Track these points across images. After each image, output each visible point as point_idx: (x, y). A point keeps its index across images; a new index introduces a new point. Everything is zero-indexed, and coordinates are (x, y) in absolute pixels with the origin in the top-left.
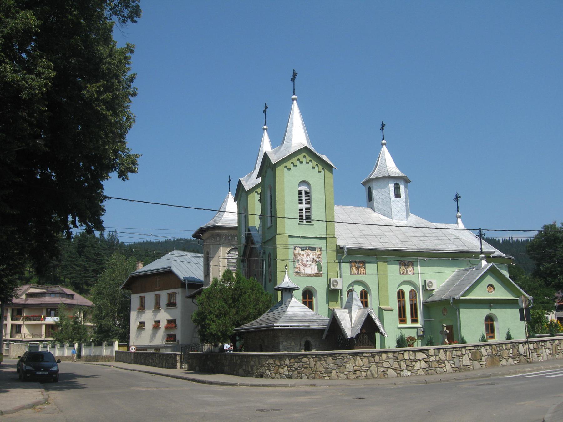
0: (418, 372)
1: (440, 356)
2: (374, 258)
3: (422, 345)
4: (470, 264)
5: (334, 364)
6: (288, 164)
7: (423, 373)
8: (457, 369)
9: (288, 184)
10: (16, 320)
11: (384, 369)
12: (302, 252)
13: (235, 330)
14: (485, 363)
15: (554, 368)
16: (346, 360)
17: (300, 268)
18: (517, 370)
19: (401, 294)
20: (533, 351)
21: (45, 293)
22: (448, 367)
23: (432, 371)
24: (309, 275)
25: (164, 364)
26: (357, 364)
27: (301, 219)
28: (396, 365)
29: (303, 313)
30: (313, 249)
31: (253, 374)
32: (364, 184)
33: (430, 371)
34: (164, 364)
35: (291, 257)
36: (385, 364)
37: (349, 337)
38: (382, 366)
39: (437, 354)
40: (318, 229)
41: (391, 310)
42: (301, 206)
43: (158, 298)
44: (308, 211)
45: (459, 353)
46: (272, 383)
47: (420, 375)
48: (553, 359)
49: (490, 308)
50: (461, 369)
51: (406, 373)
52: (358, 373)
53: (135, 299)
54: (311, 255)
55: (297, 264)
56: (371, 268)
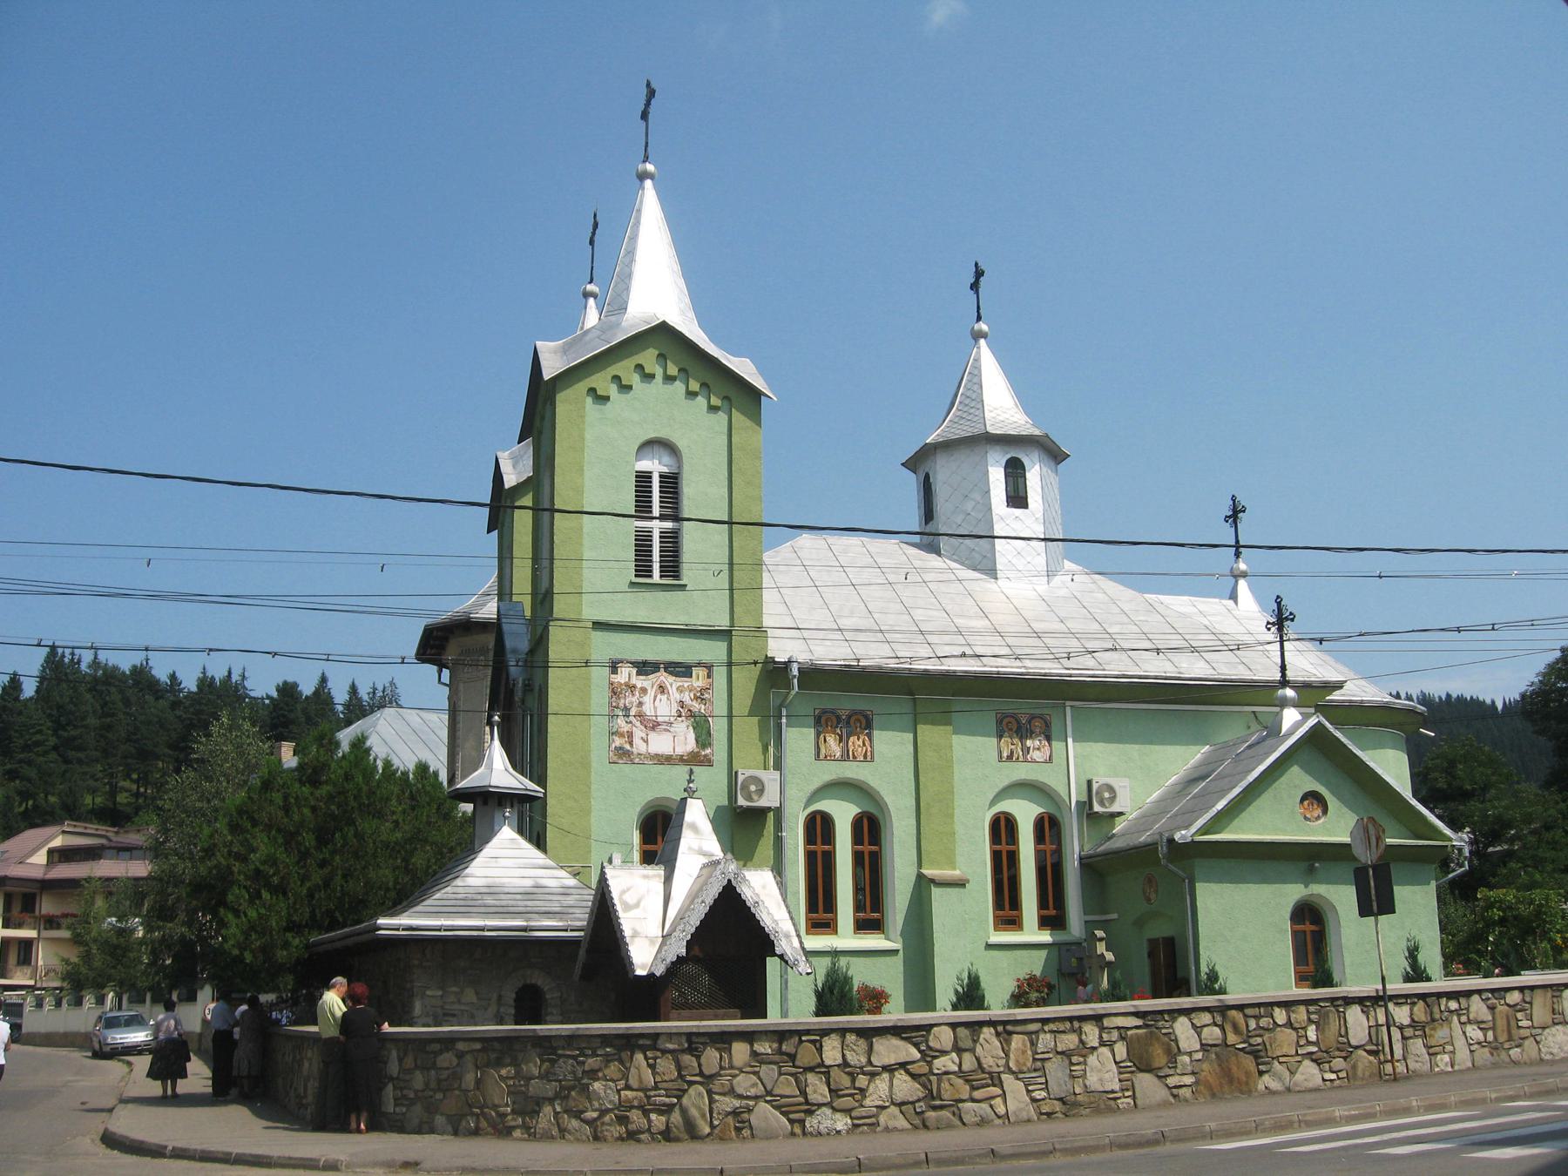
0: (882, 1119)
1: (979, 1049)
2: (902, 703)
3: (908, 1009)
7: (902, 1123)
8: (1058, 1106)
9: (604, 448)
10: (19, 926)
11: (737, 1103)
12: (639, 682)
14: (1189, 1080)
15: (1465, 1104)
16: (592, 1063)
17: (630, 735)
18: (1293, 1115)
19: (1003, 828)
20: (1409, 1032)
21: (102, 847)
23: (945, 1113)
24: (667, 760)
26: (633, 1082)
27: (643, 569)
28: (787, 1087)
29: (529, 883)
30: (681, 669)
33: (931, 1114)
35: (599, 700)
36: (744, 1083)
37: (640, 972)
38: (731, 1092)
39: (968, 1044)
40: (700, 601)
41: (960, 884)
44: (672, 542)
45: (1069, 1041)
47: (887, 1129)
49: (1309, 875)
50: (1076, 1104)
51: (827, 1120)
52: (635, 1115)
54: (673, 690)
55: (621, 721)
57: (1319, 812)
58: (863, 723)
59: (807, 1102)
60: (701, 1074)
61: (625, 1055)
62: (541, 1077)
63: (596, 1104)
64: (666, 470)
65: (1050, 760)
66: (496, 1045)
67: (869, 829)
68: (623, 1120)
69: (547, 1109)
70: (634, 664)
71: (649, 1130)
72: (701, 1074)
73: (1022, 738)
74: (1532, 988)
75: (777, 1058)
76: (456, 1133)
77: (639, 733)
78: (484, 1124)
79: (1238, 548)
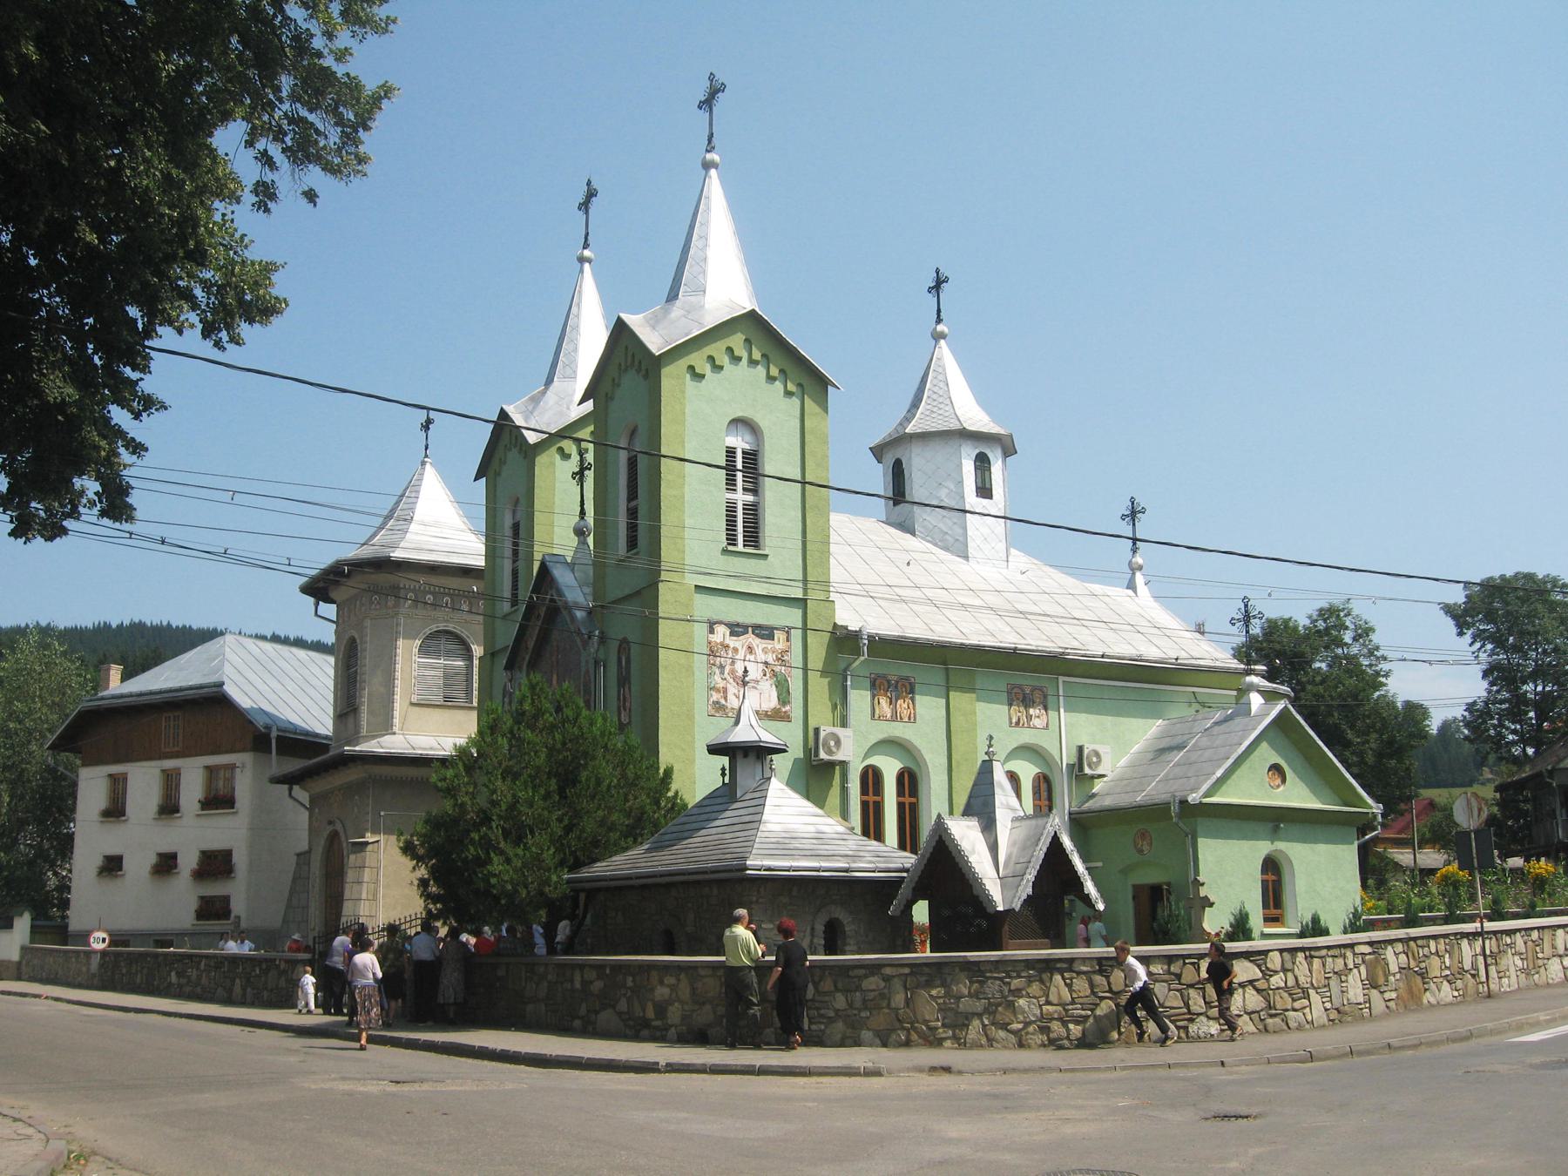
2: (935, 674)
4: (1196, 706)
5: (975, 995)
6: (698, 359)
7: (1252, 1028)
9: (700, 417)
12: (733, 642)
13: (569, 881)
16: (1016, 983)
17: (725, 690)
22: (1317, 1008)
23: (1277, 1020)
25: (237, 990)
26: (1053, 998)
27: (732, 540)
29: (812, 829)
30: (765, 632)
31: (667, 1028)
32: (878, 452)
33: (1270, 1021)
34: (237, 990)
37: (1000, 908)
42: (730, 496)
43: (171, 782)
44: (753, 511)
46: (758, 1063)
48: (1528, 988)
49: (1275, 834)
52: (1056, 1026)
53: (92, 786)
54: (759, 651)
55: (717, 678)
56: (929, 707)
57: (1279, 781)
58: (904, 689)
59: (1189, 1012)
60: (1110, 991)
61: (1045, 976)
62: (970, 995)
63: (1021, 1017)
64: (747, 447)
65: (1047, 727)
66: (926, 970)
67: (909, 782)
68: (1045, 1030)
69: (976, 1022)
70: (729, 625)
71: (1068, 1038)
72: (1110, 991)
73: (1027, 707)
74: (1543, 928)
75: (1166, 977)
76: (885, 1045)
77: (732, 689)
78: (914, 1037)
79: (1135, 540)
